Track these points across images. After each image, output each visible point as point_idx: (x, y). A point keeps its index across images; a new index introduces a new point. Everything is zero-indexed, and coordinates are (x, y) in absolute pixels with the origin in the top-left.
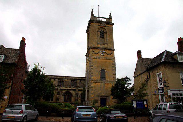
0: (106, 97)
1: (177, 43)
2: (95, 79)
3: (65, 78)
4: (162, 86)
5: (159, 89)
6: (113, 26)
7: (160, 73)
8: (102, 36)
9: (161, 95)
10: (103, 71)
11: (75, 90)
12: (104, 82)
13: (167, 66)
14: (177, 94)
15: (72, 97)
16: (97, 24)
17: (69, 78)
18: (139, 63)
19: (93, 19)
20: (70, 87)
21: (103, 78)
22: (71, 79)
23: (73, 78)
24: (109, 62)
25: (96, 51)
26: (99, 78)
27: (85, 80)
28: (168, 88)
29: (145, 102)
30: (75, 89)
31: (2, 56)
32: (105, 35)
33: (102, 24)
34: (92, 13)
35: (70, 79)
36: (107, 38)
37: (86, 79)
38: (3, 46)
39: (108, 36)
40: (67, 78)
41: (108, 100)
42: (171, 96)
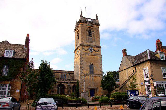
0: (95, 88)
1: (156, 44)
2: (85, 73)
3: (55, 71)
4: (148, 79)
5: (145, 81)
6: (100, 27)
7: (146, 68)
8: (90, 35)
9: (147, 86)
10: (91, 66)
11: (67, 83)
12: (92, 75)
13: (153, 63)
14: (160, 85)
15: (65, 89)
16: (86, 24)
17: (59, 72)
18: (124, 60)
19: (82, 19)
20: (63, 80)
21: (91, 72)
22: (61, 73)
23: (63, 72)
24: (97, 58)
25: (86, 48)
26: (88, 72)
27: (74, 73)
28: (154, 80)
29: (137, 92)
30: (67, 81)
31: (12, 52)
32: (93, 34)
33: (90, 25)
34: (81, 14)
35: (60, 73)
36: (94, 36)
37: (75, 73)
38: (6, 41)
39: (95, 35)
40: (58, 72)
41: (96, 91)
42: (156, 87)
